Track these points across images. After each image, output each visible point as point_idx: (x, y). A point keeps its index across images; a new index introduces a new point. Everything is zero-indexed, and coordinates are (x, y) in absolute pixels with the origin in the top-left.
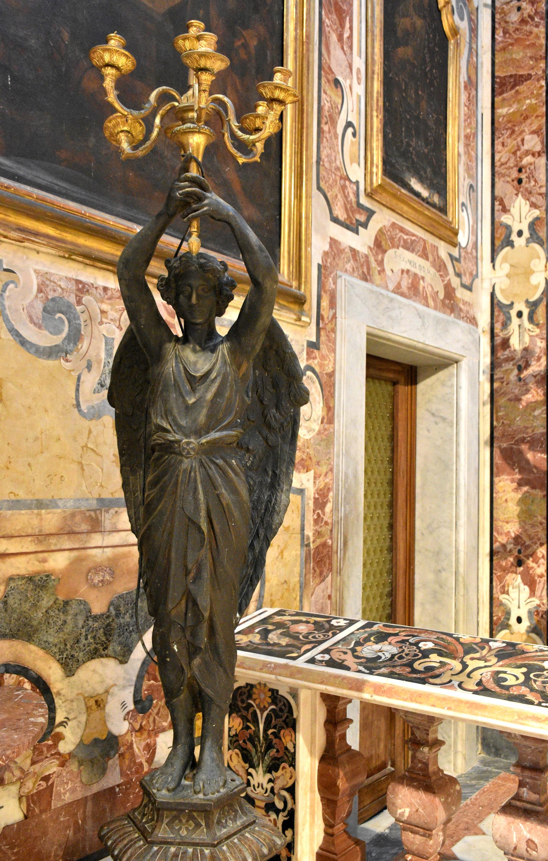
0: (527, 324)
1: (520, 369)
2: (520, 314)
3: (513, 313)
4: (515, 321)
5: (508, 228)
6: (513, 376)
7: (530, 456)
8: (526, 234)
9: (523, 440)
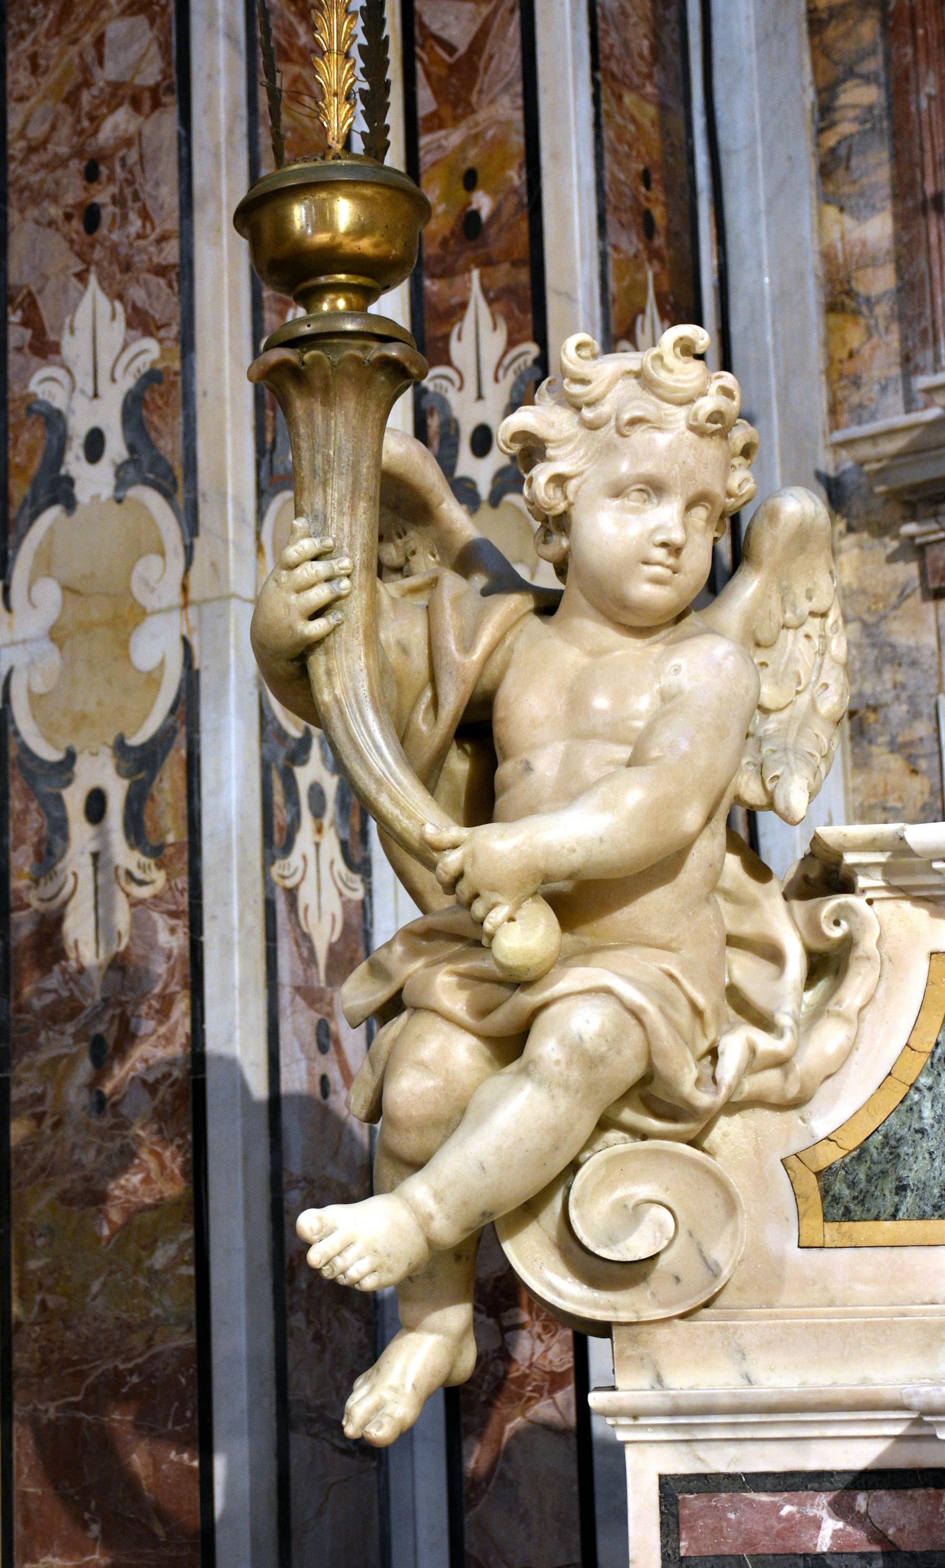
0: (125, 856)
1: (105, 1053)
2: (96, 805)
3: (74, 800)
4: (80, 832)
5: (54, 421)
6: (75, 1096)
7: (138, 1460)
8: (116, 448)
9: (112, 1388)
